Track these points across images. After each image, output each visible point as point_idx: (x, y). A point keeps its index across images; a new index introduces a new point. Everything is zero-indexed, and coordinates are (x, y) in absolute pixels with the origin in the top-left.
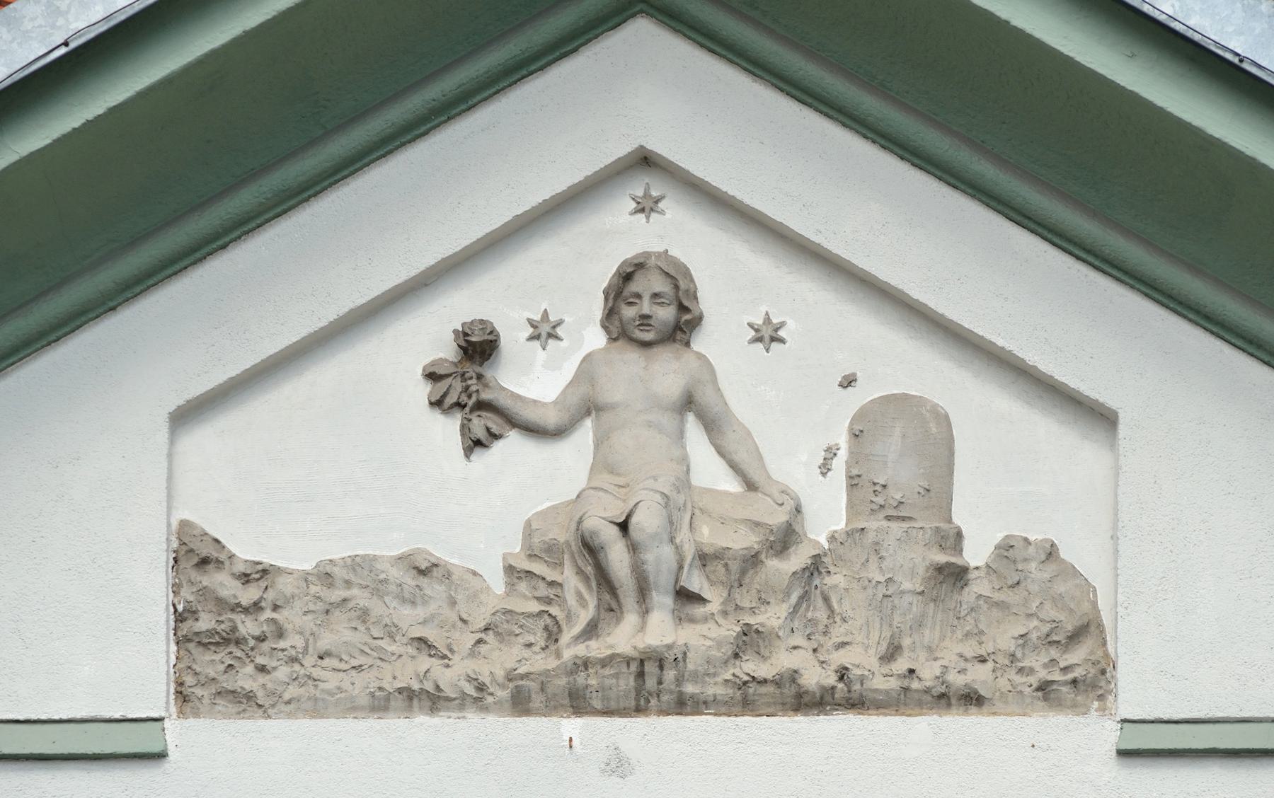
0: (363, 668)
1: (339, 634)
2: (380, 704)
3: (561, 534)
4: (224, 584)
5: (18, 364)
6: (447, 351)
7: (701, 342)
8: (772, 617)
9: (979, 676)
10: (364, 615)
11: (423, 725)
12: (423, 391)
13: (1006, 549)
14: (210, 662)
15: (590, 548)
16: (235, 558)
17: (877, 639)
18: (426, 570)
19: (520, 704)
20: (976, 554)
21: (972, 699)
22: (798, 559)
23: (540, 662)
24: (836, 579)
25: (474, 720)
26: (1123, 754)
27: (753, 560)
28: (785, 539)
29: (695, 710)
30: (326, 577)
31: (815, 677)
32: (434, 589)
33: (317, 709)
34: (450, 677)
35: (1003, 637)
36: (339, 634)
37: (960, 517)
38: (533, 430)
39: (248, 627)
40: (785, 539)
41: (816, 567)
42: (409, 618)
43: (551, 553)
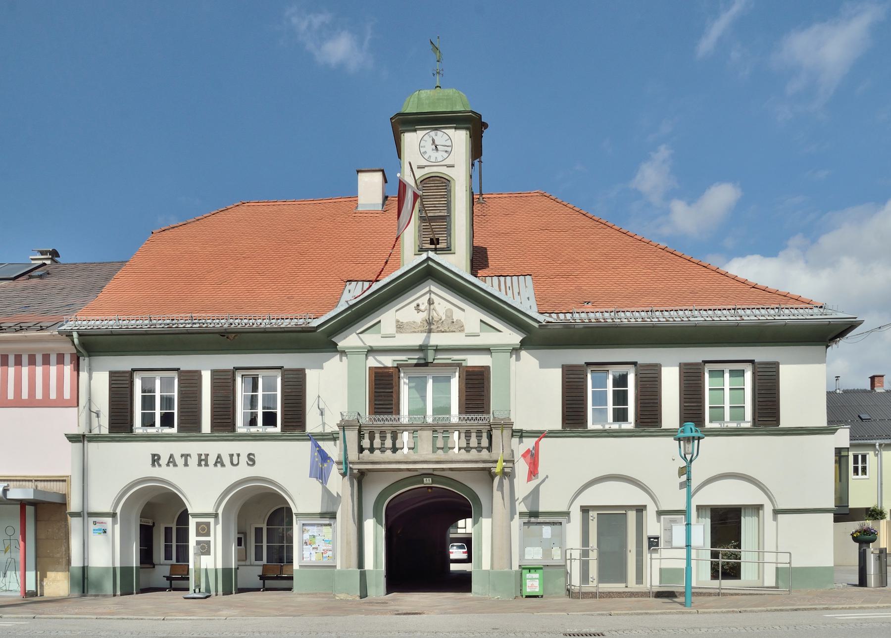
0: (540, 520)
1: (408, 327)
2: (411, 332)
3: (424, 319)
4: (400, 323)
5: (834, 611)
6: (416, 305)
7: (434, 304)
8: (440, 325)
9: (455, 330)
10: (410, 326)
11: (414, 334)
12: (414, 308)
13: (457, 320)
14: (399, 329)
15: (427, 321)
16: (829, 391)
17: (448, 327)
18: (414, 322)
19: (421, 332)
20: (454, 321)
21: (454, 332)
22: (442, 321)
23: (423, 329)
24: (444, 322)
25: (418, 334)
26: (466, 336)
27: (438, 321)
28: (441, 319)
29: (843, 453)
30: (407, 323)
31: (443, 330)
32: (415, 324)
33: (406, 333)
34: (416, 330)
35: (457, 327)
36: (408, 327)
37: (453, 318)
38: (422, 311)
39: (401, 327)
40: (441, 319)
41: (443, 322)
42: (413, 326)
43: (423, 321)
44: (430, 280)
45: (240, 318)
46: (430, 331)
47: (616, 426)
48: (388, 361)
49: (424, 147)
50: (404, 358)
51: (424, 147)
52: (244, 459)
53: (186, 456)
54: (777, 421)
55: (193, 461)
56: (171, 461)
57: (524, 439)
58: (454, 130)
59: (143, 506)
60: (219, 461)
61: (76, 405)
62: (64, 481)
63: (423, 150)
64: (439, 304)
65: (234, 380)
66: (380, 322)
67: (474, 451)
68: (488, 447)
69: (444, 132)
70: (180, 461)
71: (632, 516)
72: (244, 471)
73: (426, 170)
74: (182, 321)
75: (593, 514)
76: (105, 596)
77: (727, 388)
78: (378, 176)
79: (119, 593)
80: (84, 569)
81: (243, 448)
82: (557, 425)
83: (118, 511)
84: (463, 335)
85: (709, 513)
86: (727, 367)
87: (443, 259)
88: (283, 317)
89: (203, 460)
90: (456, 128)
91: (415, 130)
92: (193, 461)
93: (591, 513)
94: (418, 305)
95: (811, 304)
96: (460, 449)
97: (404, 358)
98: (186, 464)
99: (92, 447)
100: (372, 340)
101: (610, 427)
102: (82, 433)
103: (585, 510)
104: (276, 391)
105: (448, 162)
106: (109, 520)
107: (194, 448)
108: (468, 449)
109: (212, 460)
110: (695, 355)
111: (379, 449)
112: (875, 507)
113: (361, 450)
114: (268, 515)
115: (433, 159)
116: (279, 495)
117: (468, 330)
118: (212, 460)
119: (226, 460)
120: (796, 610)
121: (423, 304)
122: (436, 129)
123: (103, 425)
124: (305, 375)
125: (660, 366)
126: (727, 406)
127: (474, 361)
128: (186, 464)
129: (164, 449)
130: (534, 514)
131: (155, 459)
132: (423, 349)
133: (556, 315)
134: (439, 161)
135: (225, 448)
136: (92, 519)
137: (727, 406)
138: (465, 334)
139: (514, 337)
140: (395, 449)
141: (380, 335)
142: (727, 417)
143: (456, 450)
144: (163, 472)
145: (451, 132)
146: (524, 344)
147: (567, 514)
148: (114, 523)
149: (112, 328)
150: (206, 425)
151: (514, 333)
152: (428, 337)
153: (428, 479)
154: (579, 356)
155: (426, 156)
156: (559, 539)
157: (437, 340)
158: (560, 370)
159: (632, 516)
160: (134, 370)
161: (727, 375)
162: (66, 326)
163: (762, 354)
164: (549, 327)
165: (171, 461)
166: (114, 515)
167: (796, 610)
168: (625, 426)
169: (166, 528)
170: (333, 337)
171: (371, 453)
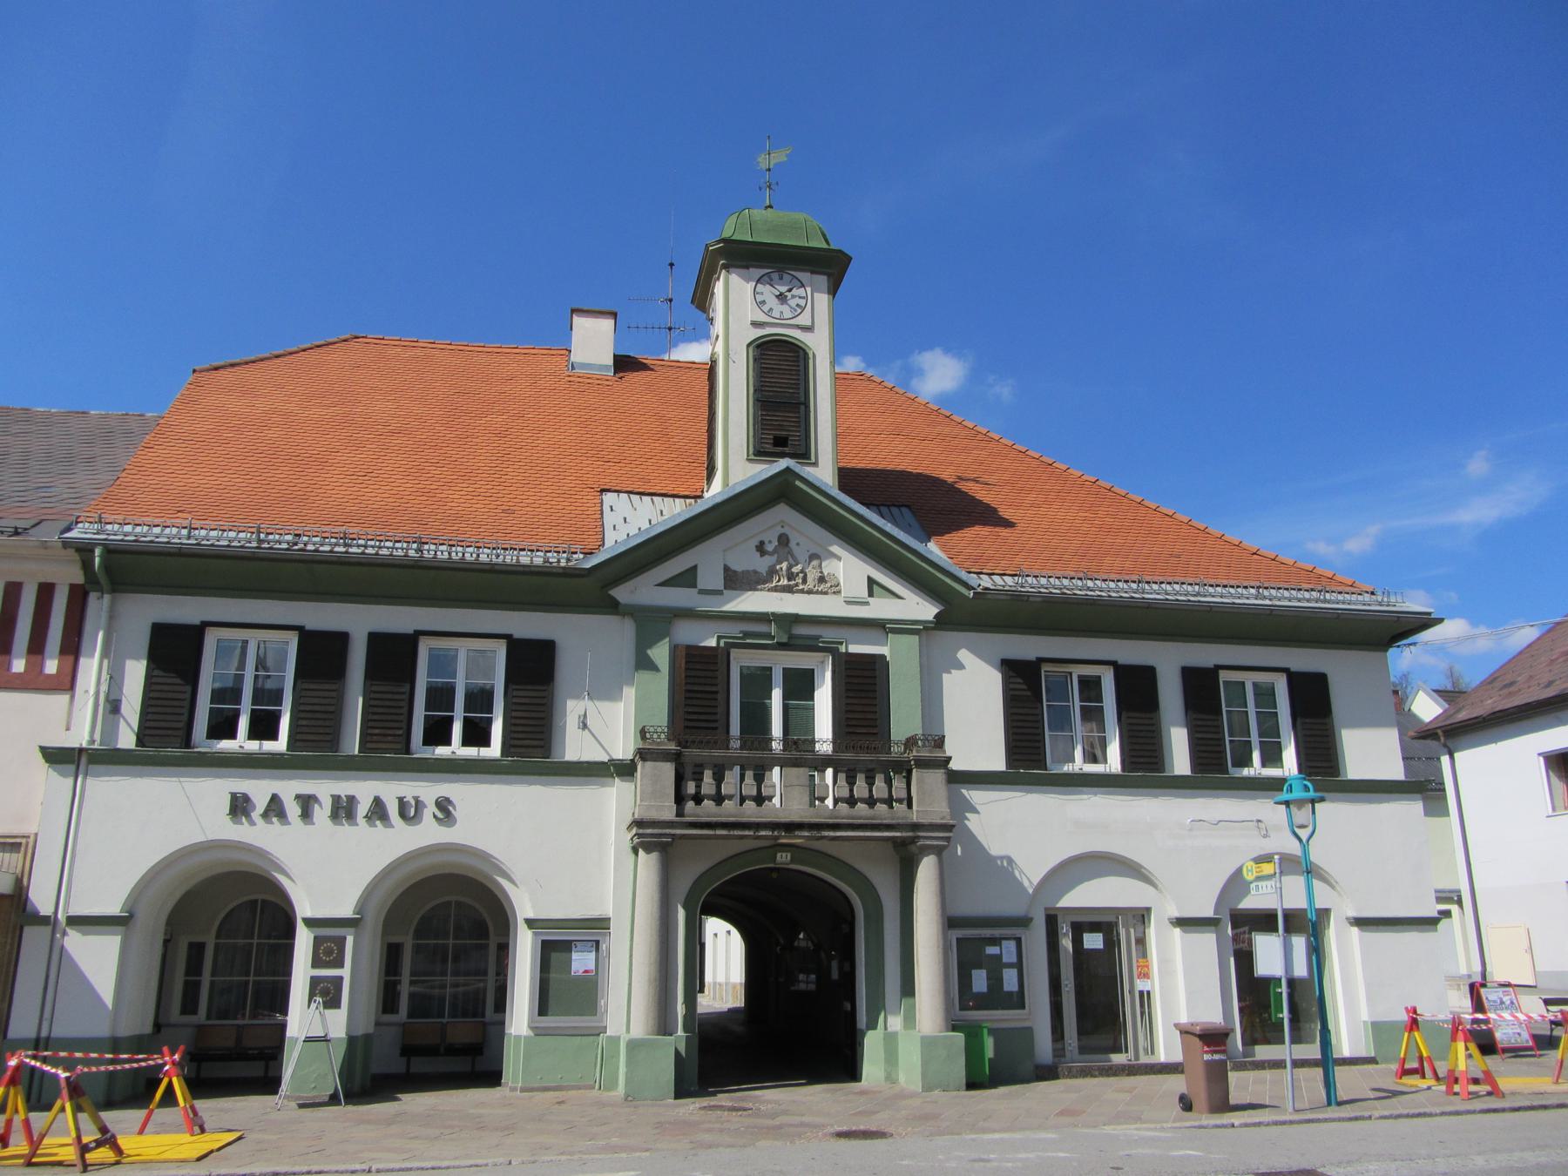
44: (782, 504)
45: (556, 549)
47: (253, 746)
49: (762, 294)
51: (762, 294)
52: (430, 809)
53: (307, 803)
55: (322, 813)
56: (275, 808)
58: (809, 274)
60: (378, 811)
61: (69, 686)
62: (14, 847)
63: (759, 298)
64: (798, 544)
67: (861, 807)
68: (755, 797)
69: (792, 275)
70: (293, 810)
72: (428, 833)
74: (389, 544)
78: (607, 324)
79: (1223, 1048)
81: (428, 790)
82: (998, 763)
84: (839, 599)
87: (808, 471)
88: (514, 547)
89: (343, 810)
90: (813, 272)
92: (322, 813)
94: (762, 543)
95: (1355, 587)
96: (836, 801)
101: (1081, 769)
102: (78, 746)
104: (1082, 707)
107: (325, 788)
108: (852, 801)
109: (363, 809)
111: (713, 799)
114: (217, 923)
115: (776, 314)
116: (271, 881)
118: (363, 809)
119: (393, 809)
120: (1357, 1118)
121: (770, 542)
131: (239, 806)
133: (1010, 578)
134: (785, 317)
135: (391, 789)
138: (843, 599)
139: (926, 610)
140: (760, 799)
143: (829, 802)
144: (258, 834)
146: (941, 622)
149: (181, 544)
150: (352, 743)
151: (925, 603)
153: (784, 855)
155: (765, 309)
162: (76, 530)
164: (989, 596)
165: (275, 808)
167: (1357, 1118)
168: (269, 746)
169: (191, 945)
170: (612, 588)
171: (758, 806)
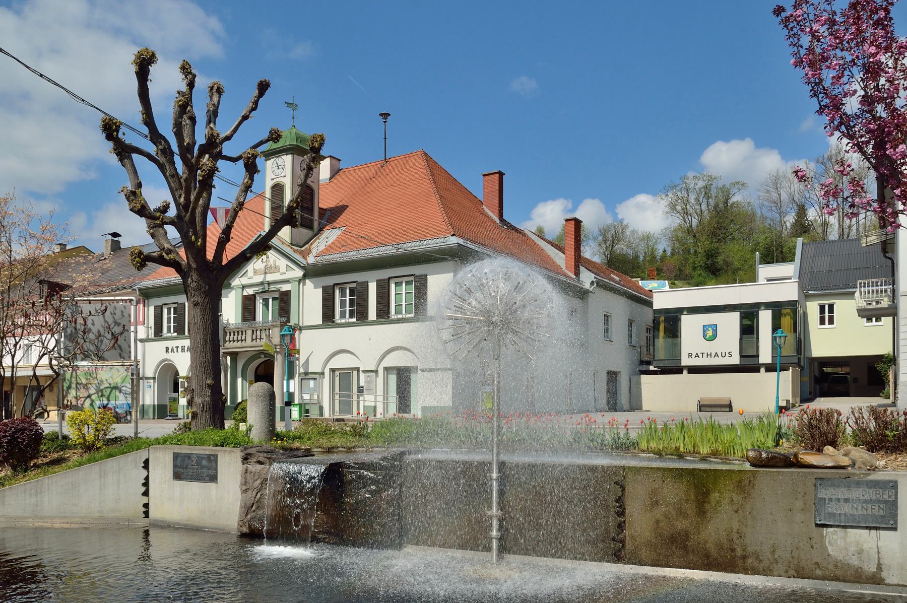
46: (266, 273)
48: (250, 291)
50: (257, 289)
53: (177, 347)
54: (367, 319)
57: (303, 331)
59: (642, 306)
65: (389, 286)
66: (247, 271)
71: (355, 372)
73: (275, 180)
75: (337, 373)
76: (149, 419)
77: (404, 292)
80: (143, 405)
82: (319, 321)
83: (157, 376)
84: (278, 274)
85: (395, 372)
86: (404, 280)
90: (286, 154)
91: (270, 159)
93: (336, 372)
97: (257, 289)
98: (177, 351)
99: (147, 344)
100: (245, 281)
103: (333, 370)
105: (283, 174)
106: (152, 381)
110: (384, 274)
112: (262, 398)
113: (253, 340)
117: (281, 271)
122: (278, 157)
123: (152, 336)
124: (368, 285)
125: (368, 282)
126: (404, 304)
127: (285, 287)
128: (177, 351)
129: (171, 344)
130: (306, 374)
132: (262, 283)
136: (146, 381)
137: (404, 304)
141: (279, 273)
142: (404, 312)
144: (170, 356)
145: (284, 157)
146: (305, 276)
147: (323, 373)
148: (154, 382)
152: (265, 277)
154: (330, 280)
156: (319, 389)
157: (270, 278)
158: (375, 283)
159: (355, 372)
160: (390, 278)
161: (404, 285)
163: (417, 270)
166: (154, 378)
